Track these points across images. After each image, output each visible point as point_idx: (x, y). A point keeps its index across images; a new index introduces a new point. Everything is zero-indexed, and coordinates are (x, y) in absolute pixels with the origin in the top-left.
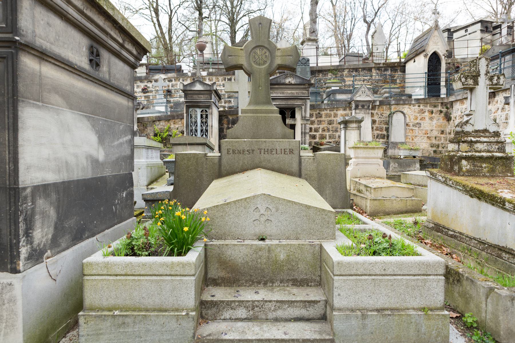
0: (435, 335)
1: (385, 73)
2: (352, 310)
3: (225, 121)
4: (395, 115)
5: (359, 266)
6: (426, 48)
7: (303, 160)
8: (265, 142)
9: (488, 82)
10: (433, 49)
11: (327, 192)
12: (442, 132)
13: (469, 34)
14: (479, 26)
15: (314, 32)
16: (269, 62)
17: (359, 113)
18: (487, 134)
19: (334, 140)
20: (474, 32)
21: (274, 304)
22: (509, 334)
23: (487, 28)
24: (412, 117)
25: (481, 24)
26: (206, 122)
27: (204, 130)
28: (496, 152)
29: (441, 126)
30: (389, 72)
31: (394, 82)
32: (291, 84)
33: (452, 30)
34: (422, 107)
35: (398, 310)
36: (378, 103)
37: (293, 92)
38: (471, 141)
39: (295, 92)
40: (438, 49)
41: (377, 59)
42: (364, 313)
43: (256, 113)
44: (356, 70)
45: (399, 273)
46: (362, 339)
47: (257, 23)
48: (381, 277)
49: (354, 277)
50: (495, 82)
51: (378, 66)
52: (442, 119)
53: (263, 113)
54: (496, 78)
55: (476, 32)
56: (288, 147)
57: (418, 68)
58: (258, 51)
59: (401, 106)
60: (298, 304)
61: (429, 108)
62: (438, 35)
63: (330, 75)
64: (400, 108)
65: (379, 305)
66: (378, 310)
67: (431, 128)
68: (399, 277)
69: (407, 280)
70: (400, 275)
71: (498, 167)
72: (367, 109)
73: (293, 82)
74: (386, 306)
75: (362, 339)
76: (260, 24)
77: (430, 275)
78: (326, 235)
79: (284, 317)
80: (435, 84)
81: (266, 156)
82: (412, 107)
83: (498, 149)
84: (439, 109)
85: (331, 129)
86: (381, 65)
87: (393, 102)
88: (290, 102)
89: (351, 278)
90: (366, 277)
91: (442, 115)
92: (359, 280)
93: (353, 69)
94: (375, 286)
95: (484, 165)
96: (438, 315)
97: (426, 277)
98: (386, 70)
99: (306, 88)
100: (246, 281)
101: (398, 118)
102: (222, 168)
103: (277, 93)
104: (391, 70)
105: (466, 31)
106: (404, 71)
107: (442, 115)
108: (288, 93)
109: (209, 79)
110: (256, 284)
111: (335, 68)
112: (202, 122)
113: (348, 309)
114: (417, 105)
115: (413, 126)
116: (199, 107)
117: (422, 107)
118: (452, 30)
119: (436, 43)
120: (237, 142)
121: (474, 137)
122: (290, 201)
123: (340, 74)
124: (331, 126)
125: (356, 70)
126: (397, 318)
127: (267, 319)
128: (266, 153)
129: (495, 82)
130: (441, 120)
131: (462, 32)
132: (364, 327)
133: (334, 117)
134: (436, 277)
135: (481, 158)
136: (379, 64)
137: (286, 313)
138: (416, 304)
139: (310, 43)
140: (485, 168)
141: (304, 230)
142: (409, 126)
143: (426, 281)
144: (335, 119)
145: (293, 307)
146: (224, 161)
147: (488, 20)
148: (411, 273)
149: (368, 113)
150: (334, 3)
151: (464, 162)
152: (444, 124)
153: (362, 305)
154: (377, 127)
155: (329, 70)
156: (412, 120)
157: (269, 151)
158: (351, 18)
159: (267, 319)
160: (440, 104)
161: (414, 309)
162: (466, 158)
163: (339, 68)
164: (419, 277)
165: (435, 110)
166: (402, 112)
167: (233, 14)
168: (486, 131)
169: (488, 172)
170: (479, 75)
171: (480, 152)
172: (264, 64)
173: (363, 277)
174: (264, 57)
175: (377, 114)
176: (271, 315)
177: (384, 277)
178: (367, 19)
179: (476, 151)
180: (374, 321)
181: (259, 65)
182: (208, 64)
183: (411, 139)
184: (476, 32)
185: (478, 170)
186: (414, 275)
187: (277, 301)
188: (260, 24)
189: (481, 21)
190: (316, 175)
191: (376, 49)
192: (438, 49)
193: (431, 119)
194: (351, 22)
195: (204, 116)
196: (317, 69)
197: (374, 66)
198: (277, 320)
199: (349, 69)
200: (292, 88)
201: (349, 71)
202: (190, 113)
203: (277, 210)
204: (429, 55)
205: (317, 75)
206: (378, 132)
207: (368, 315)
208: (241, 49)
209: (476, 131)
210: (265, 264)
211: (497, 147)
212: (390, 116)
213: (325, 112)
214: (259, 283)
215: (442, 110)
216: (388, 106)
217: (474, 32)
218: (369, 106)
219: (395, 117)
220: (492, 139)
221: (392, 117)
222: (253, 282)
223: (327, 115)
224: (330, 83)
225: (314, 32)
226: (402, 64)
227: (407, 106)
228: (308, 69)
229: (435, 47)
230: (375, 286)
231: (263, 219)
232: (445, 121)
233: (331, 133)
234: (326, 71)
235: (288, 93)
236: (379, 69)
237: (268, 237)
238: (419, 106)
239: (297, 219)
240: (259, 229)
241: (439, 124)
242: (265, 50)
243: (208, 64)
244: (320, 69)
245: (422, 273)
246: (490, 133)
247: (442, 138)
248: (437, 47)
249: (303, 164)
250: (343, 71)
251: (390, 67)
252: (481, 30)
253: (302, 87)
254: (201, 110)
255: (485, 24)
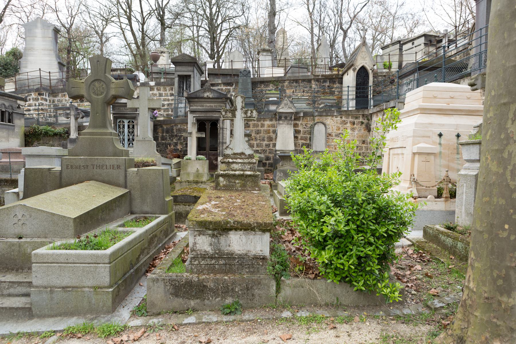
0: (102, 305)
1: (324, 84)
2: (46, 287)
3: (160, 130)
4: (316, 125)
5: (49, 257)
6: (355, 62)
7: (128, 174)
8: (97, 159)
9: (243, 115)
10: (361, 63)
11: (148, 200)
12: (364, 142)
13: (415, 47)
14: (422, 40)
15: (272, 42)
16: (105, 93)
17: (282, 124)
18: (243, 156)
19: (261, 148)
20: (419, 45)
21: (7, 284)
22: (152, 305)
23: (431, 41)
24: (335, 128)
25: (425, 38)
26: (133, 132)
27: (131, 139)
28: (249, 171)
29: (362, 136)
30: (327, 84)
31: (332, 93)
32: (209, 98)
33: (401, 43)
34: (344, 119)
35: (77, 287)
36: (302, 115)
37: (212, 105)
38: (229, 162)
39: (213, 105)
40: (366, 63)
41: (322, 70)
42: (51, 289)
43: (93, 135)
44: (296, 81)
45: (77, 261)
46: (51, 308)
47: (95, 61)
48: (65, 265)
49: (47, 265)
50: (249, 115)
51: (317, 78)
52: (363, 130)
53: (99, 135)
54: (249, 112)
55: (420, 45)
56: (115, 163)
57: (350, 79)
58: (97, 84)
59: (324, 117)
60: (25, 284)
61: (350, 119)
62: (365, 50)
63: (271, 87)
64: (323, 119)
65: (64, 284)
66: (63, 288)
67: (352, 138)
68: (78, 265)
69: (83, 267)
70: (78, 263)
71: (248, 183)
72: (289, 120)
73: (211, 96)
74: (69, 285)
75: (51, 308)
76: (98, 61)
77: (99, 263)
78: (66, 235)
79: (15, 293)
80: (364, 97)
81: (98, 171)
82: (334, 118)
83: (250, 168)
84: (361, 120)
85: (258, 138)
86: (320, 77)
87: (316, 114)
88: (209, 115)
89: (45, 265)
90: (55, 265)
91: (364, 126)
92: (50, 266)
93: (293, 80)
94: (60, 271)
95: (237, 181)
96: (103, 291)
97: (96, 265)
98: (325, 81)
99: (223, 102)
100: (3, 268)
101: (319, 129)
102: (63, 180)
103: (197, 106)
104: (330, 82)
105: (413, 44)
106: (341, 83)
107: (364, 126)
108: (207, 106)
109: (157, 89)
110: (10, 271)
111: (277, 79)
112: (129, 132)
113: (42, 287)
114: (339, 117)
115: (336, 136)
116: (126, 118)
117: (344, 119)
118: (401, 43)
119: (364, 59)
120: (74, 159)
121: (232, 159)
122: (39, 210)
123: (281, 84)
124: (258, 135)
125: (296, 81)
126: (74, 293)
127: (3, 295)
128: (98, 168)
129: (249, 115)
130: (363, 131)
131: (409, 45)
132: (52, 299)
133: (261, 127)
134: (104, 265)
135: (234, 176)
136: (318, 76)
137: (16, 290)
138: (90, 284)
139: (265, 54)
140: (238, 183)
141: (51, 231)
142: (332, 136)
143: (96, 267)
144: (262, 129)
145: (21, 286)
146: (64, 175)
147: (431, 34)
148: (86, 262)
149: (291, 124)
150: (311, 11)
151: (221, 179)
152: (365, 134)
153: (52, 284)
154: (302, 137)
155: (271, 81)
156: (335, 131)
157: (101, 167)
158: (334, 24)
159: (3, 295)
160: (361, 116)
161: (88, 287)
162: (222, 176)
163: (280, 79)
164: (92, 265)
165: (356, 121)
166: (325, 125)
167: (212, 20)
168: (243, 153)
169: (241, 186)
170: (236, 110)
171: (235, 170)
172: (101, 94)
173: (53, 265)
174: (101, 89)
175: (301, 124)
176: (5, 292)
177: (68, 265)
178: (343, 27)
179: (232, 170)
180: (59, 295)
181: (97, 95)
182: (160, 73)
183: (334, 148)
184: (420, 45)
185: (233, 185)
186: (89, 264)
187: (10, 282)
188: (98, 61)
189: (425, 35)
190: (139, 187)
191: (321, 61)
192: (366, 63)
193: (353, 129)
194: (335, 28)
195: (131, 127)
196: (259, 80)
197: (313, 77)
198: (9, 295)
199: (290, 80)
200: (211, 102)
201: (289, 83)
202: (118, 124)
203: (31, 217)
204: (358, 69)
205: (259, 86)
206: (303, 141)
207: (54, 291)
208: (82, 82)
209: (235, 154)
210: (17, 256)
211: (249, 167)
212: (312, 127)
213: (253, 122)
214: (13, 270)
215: (364, 121)
216: (312, 117)
217: (419, 45)
218: (292, 117)
219: (316, 128)
220: (246, 161)
221: (313, 128)
222: (8, 269)
223: (255, 126)
224: (270, 94)
225: (272, 42)
226: (340, 77)
227: (330, 118)
228: (249, 81)
229: (363, 61)
230: (60, 271)
231: (20, 223)
232: (366, 132)
233: (258, 142)
234: (267, 82)
235: (207, 106)
236: (318, 80)
237: (25, 236)
238: (341, 118)
239: (45, 223)
240: (18, 230)
241: (360, 134)
242: (102, 83)
243: (160, 73)
244: (262, 80)
245: (94, 262)
246: (246, 155)
247: (364, 148)
248: (365, 62)
249: (128, 178)
250: (284, 82)
251: (329, 79)
252: (425, 43)
253: (220, 100)
254: (128, 121)
255: (429, 38)
